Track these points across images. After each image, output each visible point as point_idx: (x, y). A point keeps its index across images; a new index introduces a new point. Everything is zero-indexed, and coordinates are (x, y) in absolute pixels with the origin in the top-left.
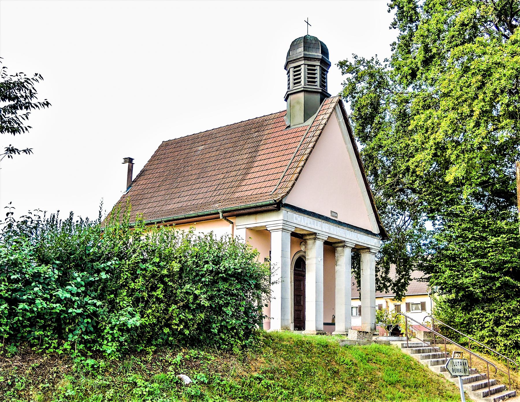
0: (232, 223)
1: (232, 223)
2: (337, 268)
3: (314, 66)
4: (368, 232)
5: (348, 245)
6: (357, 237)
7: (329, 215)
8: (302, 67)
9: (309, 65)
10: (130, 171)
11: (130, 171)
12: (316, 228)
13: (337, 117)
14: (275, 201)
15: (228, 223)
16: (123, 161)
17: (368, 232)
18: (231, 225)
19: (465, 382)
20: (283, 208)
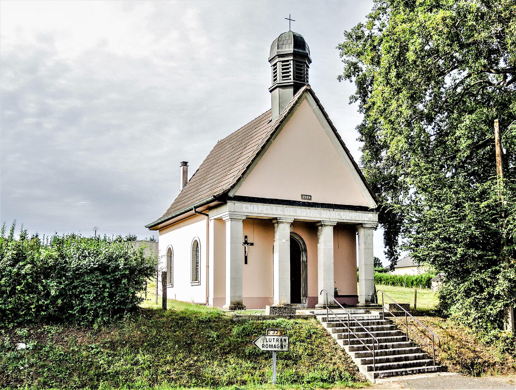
0: (208, 215)
1: (208, 215)
2: (319, 245)
3: (288, 61)
4: (364, 209)
5: (326, 224)
6: (339, 215)
7: (299, 199)
8: (278, 64)
9: (283, 62)
10: (185, 173)
11: (185, 173)
12: (275, 212)
13: (310, 105)
14: (214, 196)
15: (203, 216)
16: (180, 165)
17: (364, 209)
18: (206, 217)
19: (346, 343)
20: (228, 201)
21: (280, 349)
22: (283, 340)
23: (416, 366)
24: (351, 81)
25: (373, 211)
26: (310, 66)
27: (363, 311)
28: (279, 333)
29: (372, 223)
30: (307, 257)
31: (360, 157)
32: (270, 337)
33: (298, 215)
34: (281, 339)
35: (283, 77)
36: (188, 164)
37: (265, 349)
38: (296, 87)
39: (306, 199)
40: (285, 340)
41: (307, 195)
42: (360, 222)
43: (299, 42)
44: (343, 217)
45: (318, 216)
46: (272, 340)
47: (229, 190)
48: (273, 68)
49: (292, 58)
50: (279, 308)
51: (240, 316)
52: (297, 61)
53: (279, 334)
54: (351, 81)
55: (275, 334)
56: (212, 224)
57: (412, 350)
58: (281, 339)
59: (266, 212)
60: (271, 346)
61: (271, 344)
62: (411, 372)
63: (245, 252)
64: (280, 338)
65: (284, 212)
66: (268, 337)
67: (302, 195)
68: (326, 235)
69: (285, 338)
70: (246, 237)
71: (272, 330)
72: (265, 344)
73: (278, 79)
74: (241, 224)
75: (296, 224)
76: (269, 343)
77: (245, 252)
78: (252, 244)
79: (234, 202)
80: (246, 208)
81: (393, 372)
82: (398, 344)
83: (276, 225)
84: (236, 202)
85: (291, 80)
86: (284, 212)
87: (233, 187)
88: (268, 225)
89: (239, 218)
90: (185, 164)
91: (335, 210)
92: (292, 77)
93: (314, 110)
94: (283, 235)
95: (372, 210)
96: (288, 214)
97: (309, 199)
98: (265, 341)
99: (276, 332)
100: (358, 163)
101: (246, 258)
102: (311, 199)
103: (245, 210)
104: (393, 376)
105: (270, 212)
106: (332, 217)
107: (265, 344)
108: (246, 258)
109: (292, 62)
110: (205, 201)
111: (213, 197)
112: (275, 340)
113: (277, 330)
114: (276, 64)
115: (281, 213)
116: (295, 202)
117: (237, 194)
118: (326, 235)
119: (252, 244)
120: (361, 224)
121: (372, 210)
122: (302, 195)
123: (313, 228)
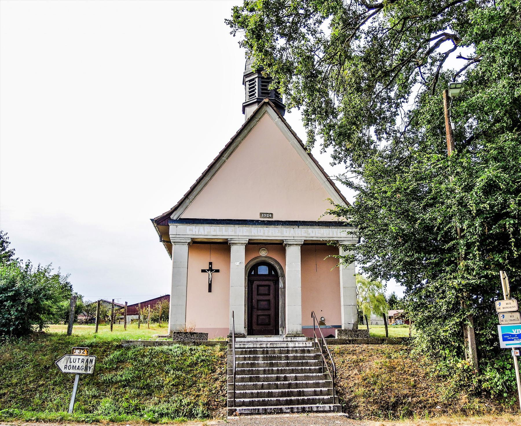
3: (253, 79)
5: (289, 243)
7: (257, 218)
21: (83, 372)
22: (89, 361)
23: (307, 404)
33: (253, 234)
34: (87, 360)
40: (91, 361)
45: (279, 234)
46: (77, 360)
49: (257, 76)
50: (185, 333)
51: (131, 342)
55: (81, 354)
57: (319, 383)
58: (87, 360)
59: (214, 234)
61: (74, 364)
62: (288, 411)
64: (86, 358)
65: (235, 232)
66: (72, 357)
67: (261, 214)
68: (293, 255)
69: (91, 358)
70: (211, 263)
71: (77, 349)
72: (68, 364)
74: (186, 247)
75: (252, 245)
76: (72, 364)
78: (217, 271)
79: (176, 224)
80: (190, 230)
81: (259, 409)
82: (305, 376)
84: (178, 225)
86: (235, 232)
87: (176, 209)
88: (224, 247)
89: (182, 241)
91: (300, 227)
93: (276, 124)
94: (239, 258)
96: (241, 234)
97: (269, 217)
98: (69, 361)
99: (82, 351)
101: (210, 285)
102: (272, 217)
103: (189, 232)
104: (259, 414)
106: (297, 235)
107: (68, 364)
108: (210, 285)
109: (257, 80)
112: (80, 360)
113: (83, 349)
115: (233, 234)
118: (293, 255)
119: (217, 271)
122: (261, 214)
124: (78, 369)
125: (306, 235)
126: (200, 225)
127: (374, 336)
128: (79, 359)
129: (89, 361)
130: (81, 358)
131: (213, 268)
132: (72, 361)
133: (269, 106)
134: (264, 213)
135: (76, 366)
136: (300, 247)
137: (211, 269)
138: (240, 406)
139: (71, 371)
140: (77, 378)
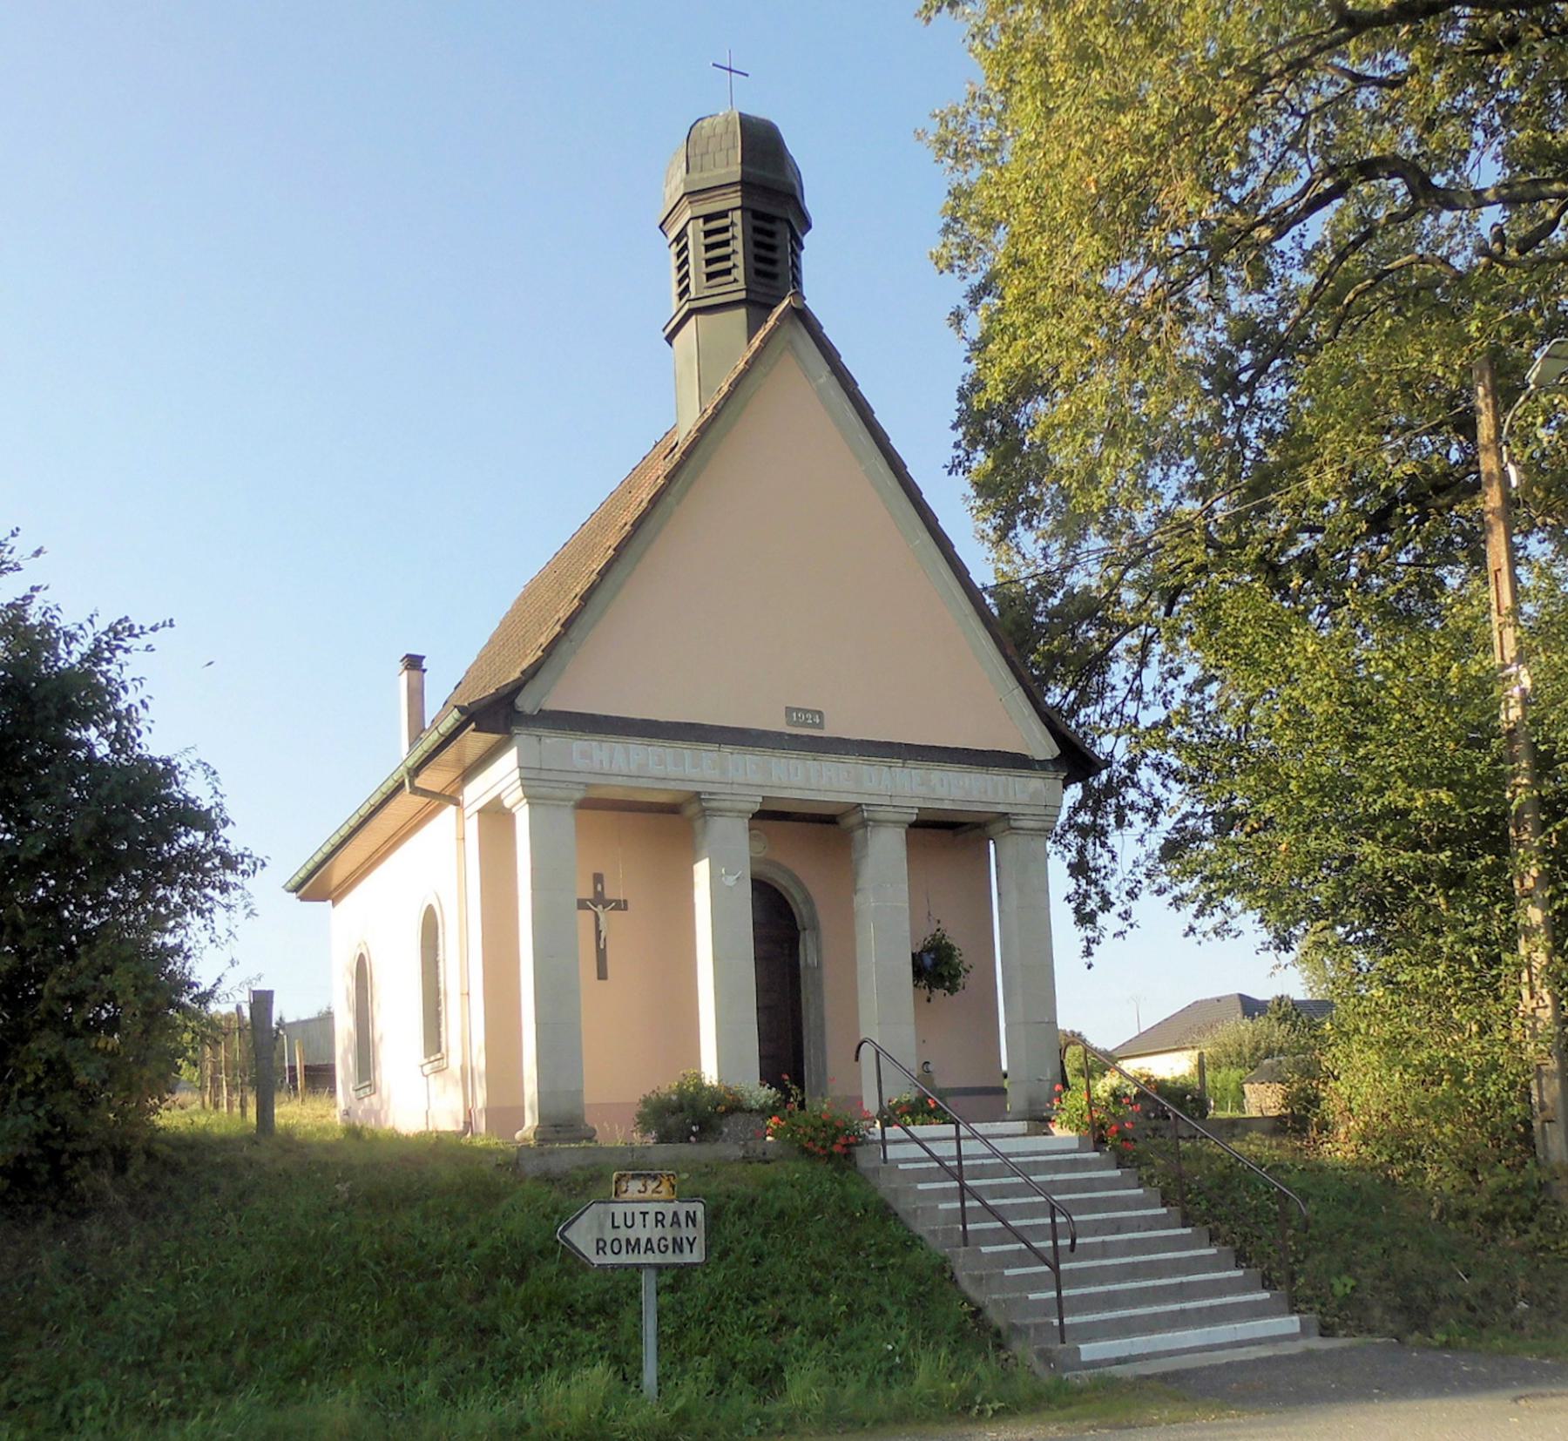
4: (1018, 762)
7: (779, 725)
9: (708, 218)
12: (691, 772)
14: (461, 709)
16: (401, 666)
17: (1018, 762)
22: (682, 1218)
24: (968, 360)
25: (1044, 769)
26: (807, 240)
27: (1021, 1126)
28: (665, 1188)
29: (1041, 811)
30: (819, 951)
31: (931, 155)
32: (629, 1208)
35: (710, 276)
36: (425, 664)
37: (610, 1259)
38: (757, 304)
39: (805, 725)
41: (806, 711)
42: (1001, 809)
43: (762, 145)
44: (941, 792)
46: (639, 1218)
47: (517, 687)
48: (675, 249)
52: (757, 215)
53: (664, 1195)
54: (968, 360)
55: (648, 1195)
56: (472, 826)
58: (675, 1214)
59: (657, 771)
60: (633, 1246)
61: (632, 1235)
63: (598, 933)
66: (619, 1209)
68: (885, 853)
69: (690, 1207)
70: (598, 878)
71: (634, 1177)
73: (692, 288)
75: (770, 816)
76: (623, 1233)
77: (598, 933)
78: (621, 906)
79: (540, 732)
83: (698, 824)
85: (736, 284)
88: (672, 821)
89: (558, 793)
90: (414, 663)
92: (739, 273)
95: (1042, 765)
97: (814, 725)
99: (652, 1185)
100: (1067, 1070)
102: (820, 726)
105: (672, 771)
110: (435, 736)
111: (456, 714)
112: (650, 1219)
113: (655, 1178)
114: (682, 234)
115: (714, 774)
116: (765, 734)
117: (551, 704)
118: (885, 853)
119: (621, 906)
120: (1005, 816)
121: (1042, 765)
123: (828, 828)
124: (649, 1248)
125: (923, 791)
126: (614, 738)
127: (289, 1134)
128: (644, 1214)
129: (682, 1218)
130: (652, 1208)
131: (608, 895)
132: (619, 1221)
133: (800, 325)
134: (798, 710)
135: (638, 1240)
136: (903, 832)
137: (599, 899)
138: (1086, 1368)
139: (625, 1258)
140: (648, 1283)
